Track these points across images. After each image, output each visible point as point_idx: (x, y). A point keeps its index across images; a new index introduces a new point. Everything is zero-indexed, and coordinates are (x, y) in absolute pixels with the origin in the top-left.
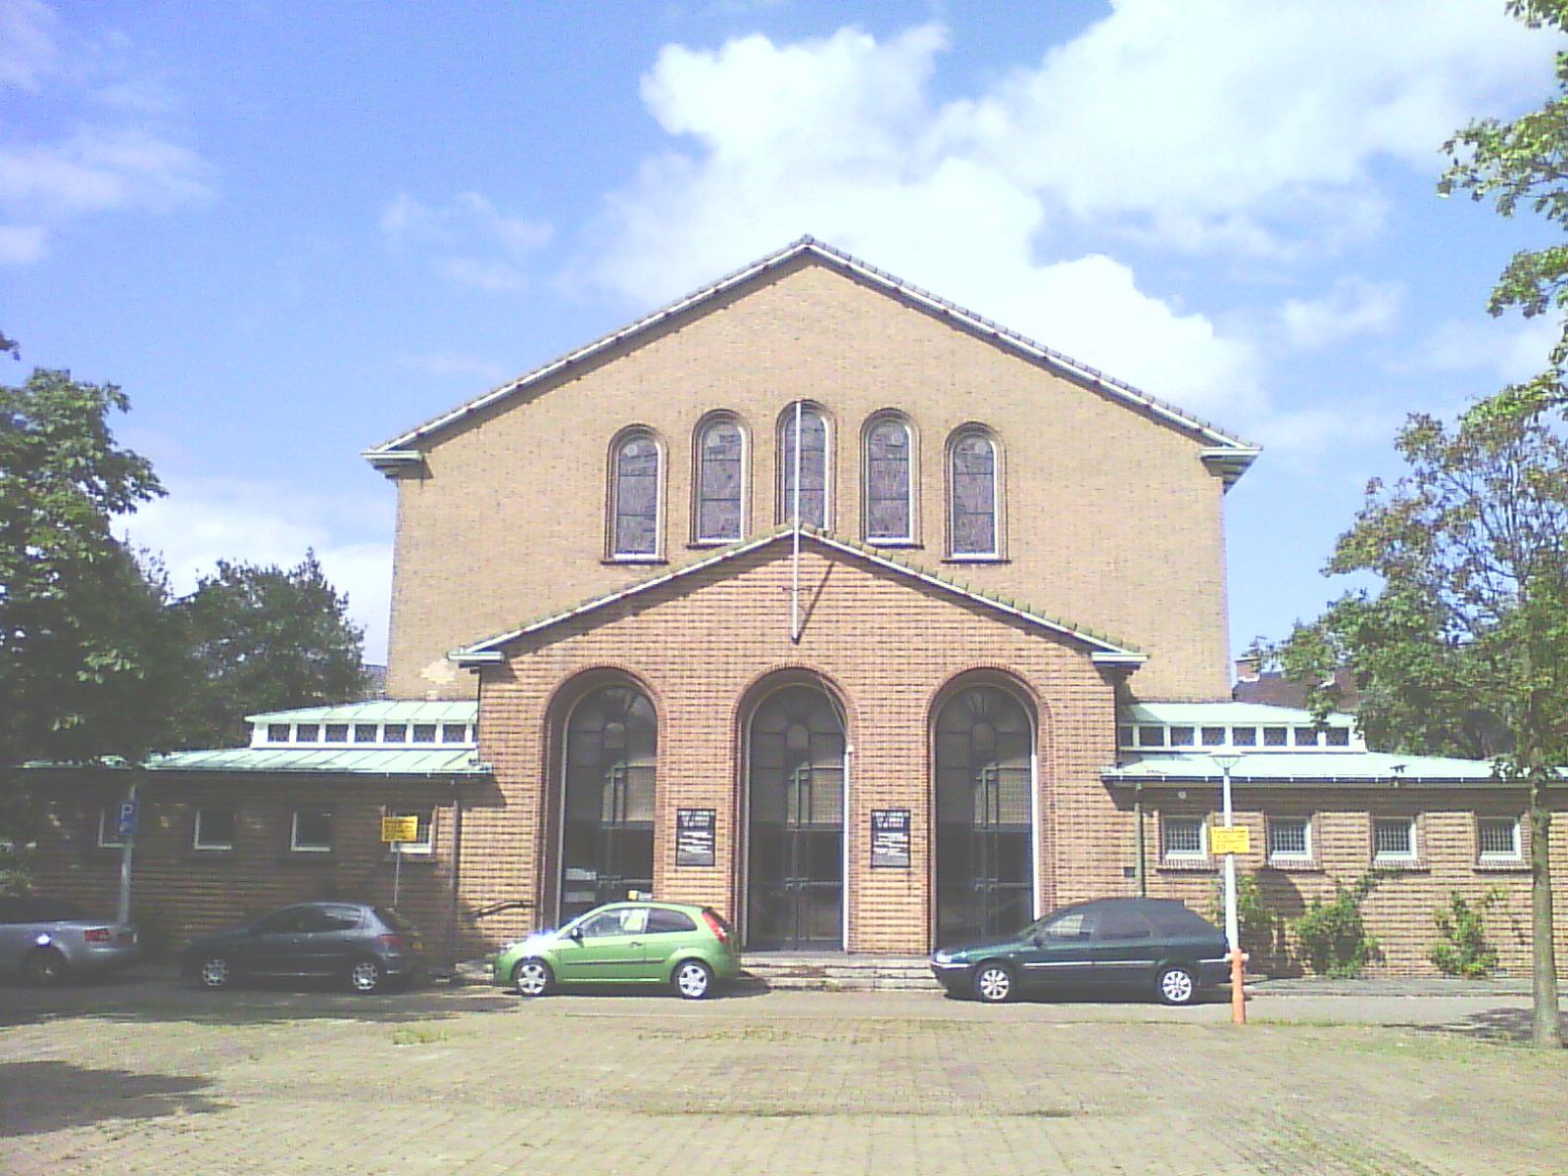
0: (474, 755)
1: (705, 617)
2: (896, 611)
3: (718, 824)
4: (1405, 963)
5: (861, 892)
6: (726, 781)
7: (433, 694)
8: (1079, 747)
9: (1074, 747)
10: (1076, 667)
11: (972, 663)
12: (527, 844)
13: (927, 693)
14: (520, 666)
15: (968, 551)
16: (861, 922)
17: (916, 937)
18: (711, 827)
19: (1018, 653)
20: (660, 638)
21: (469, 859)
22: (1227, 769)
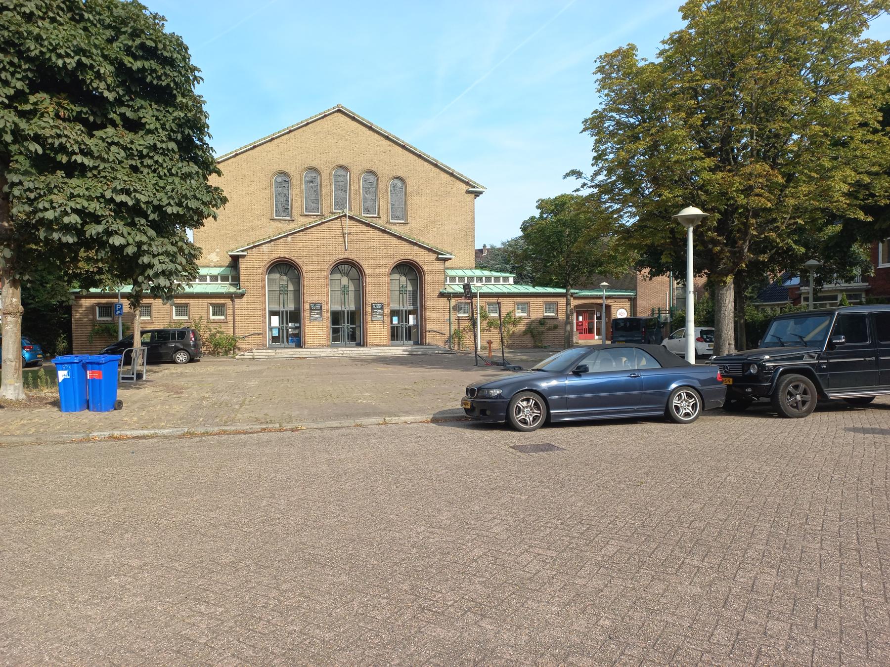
7: (212, 264)
18: (321, 309)
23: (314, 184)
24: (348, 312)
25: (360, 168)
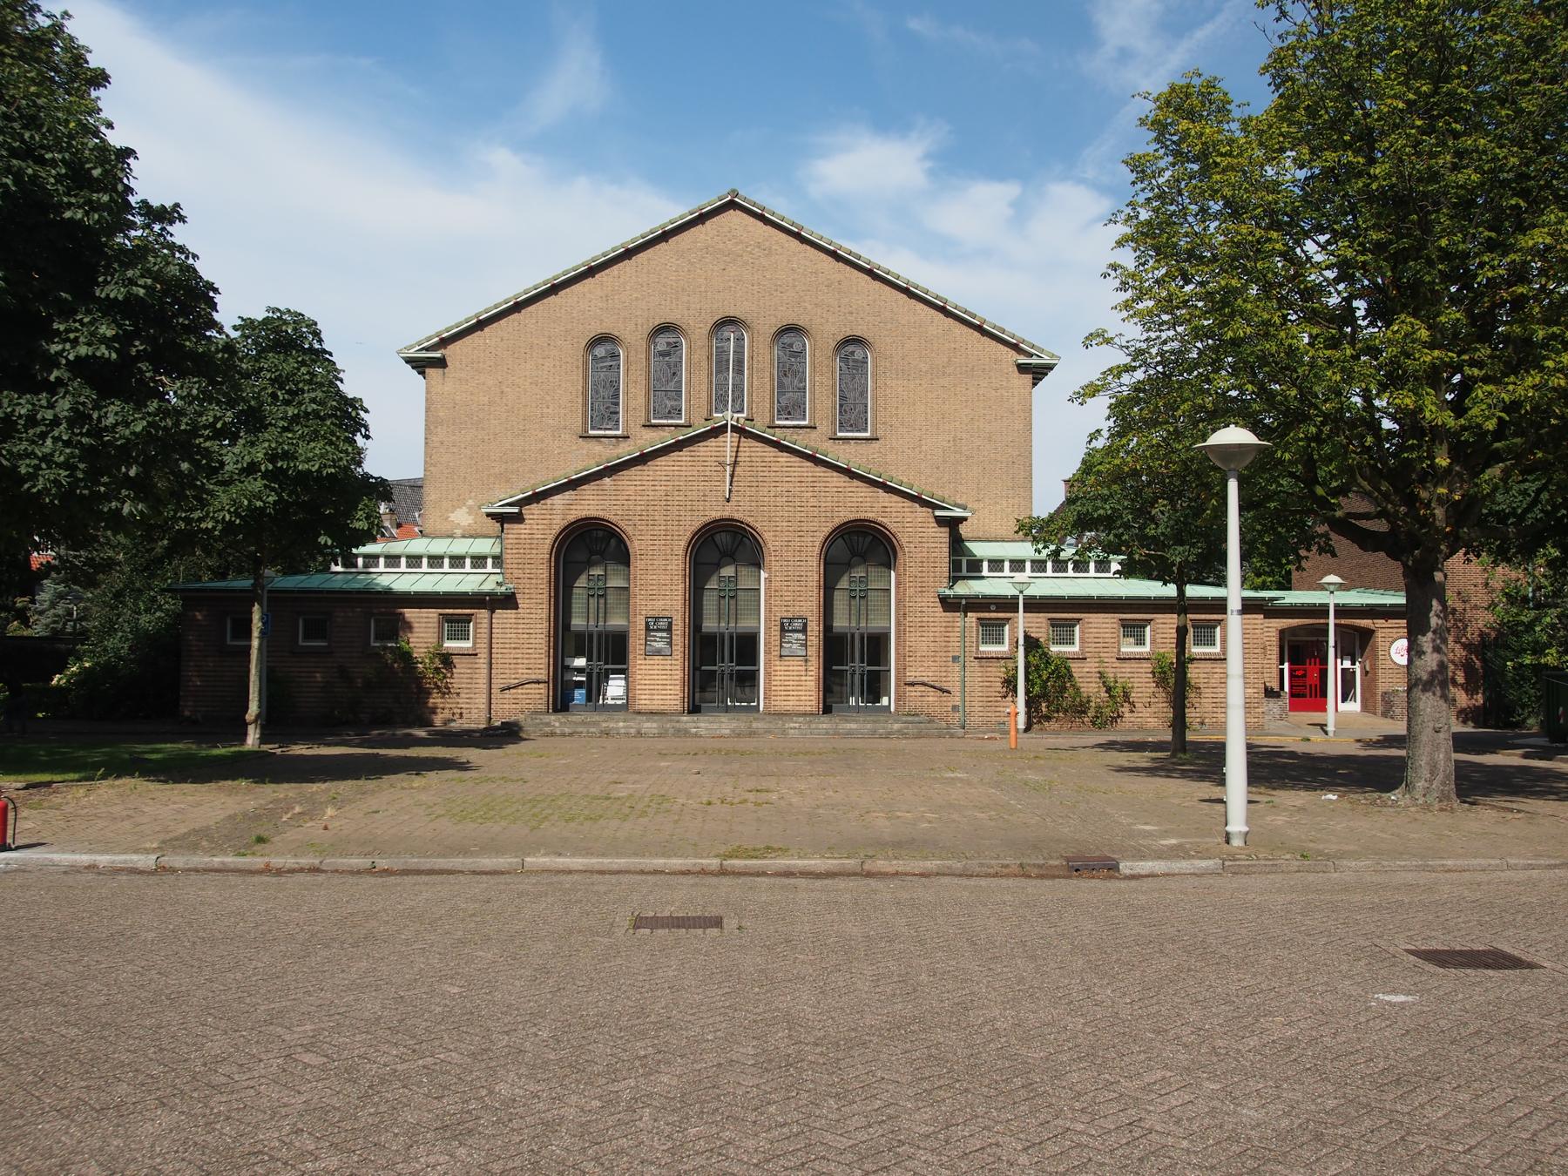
0: (500, 578)
1: (663, 483)
2: (799, 479)
3: (674, 627)
4: (1139, 720)
5: (773, 673)
6: (679, 598)
7: (458, 532)
8: (924, 574)
9: (920, 575)
10: (923, 520)
11: (852, 516)
12: (541, 641)
13: (821, 537)
14: (531, 517)
15: (848, 431)
16: (773, 693)
17: (810, 703)
18: (669, 629)
19: (883, 509)
20: (631, 498)
21: (500, 651)
22: (1021, 592)
23: (673, 359)
24: (731, 638)
25: (773, 320)
